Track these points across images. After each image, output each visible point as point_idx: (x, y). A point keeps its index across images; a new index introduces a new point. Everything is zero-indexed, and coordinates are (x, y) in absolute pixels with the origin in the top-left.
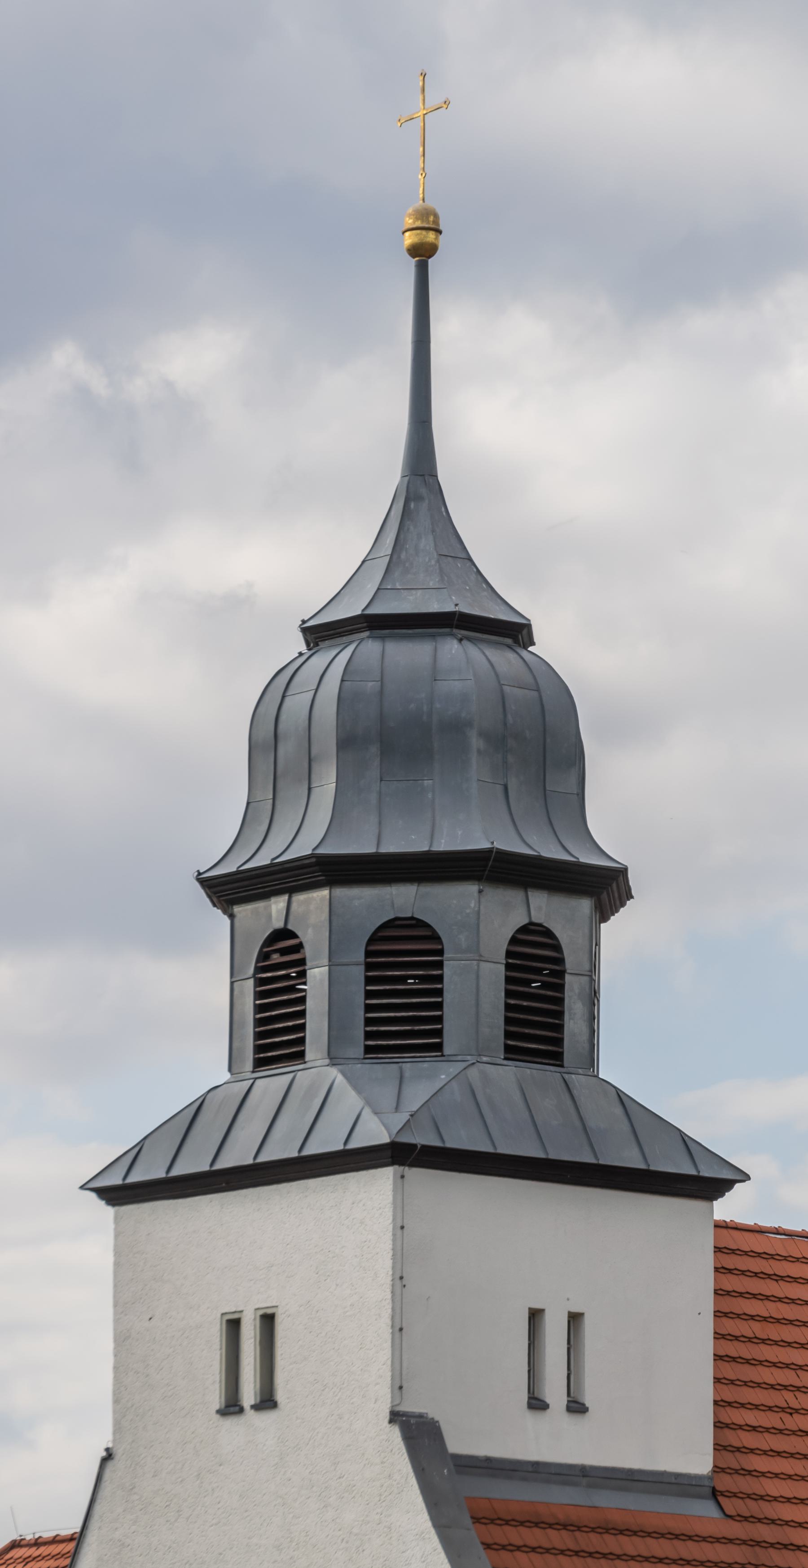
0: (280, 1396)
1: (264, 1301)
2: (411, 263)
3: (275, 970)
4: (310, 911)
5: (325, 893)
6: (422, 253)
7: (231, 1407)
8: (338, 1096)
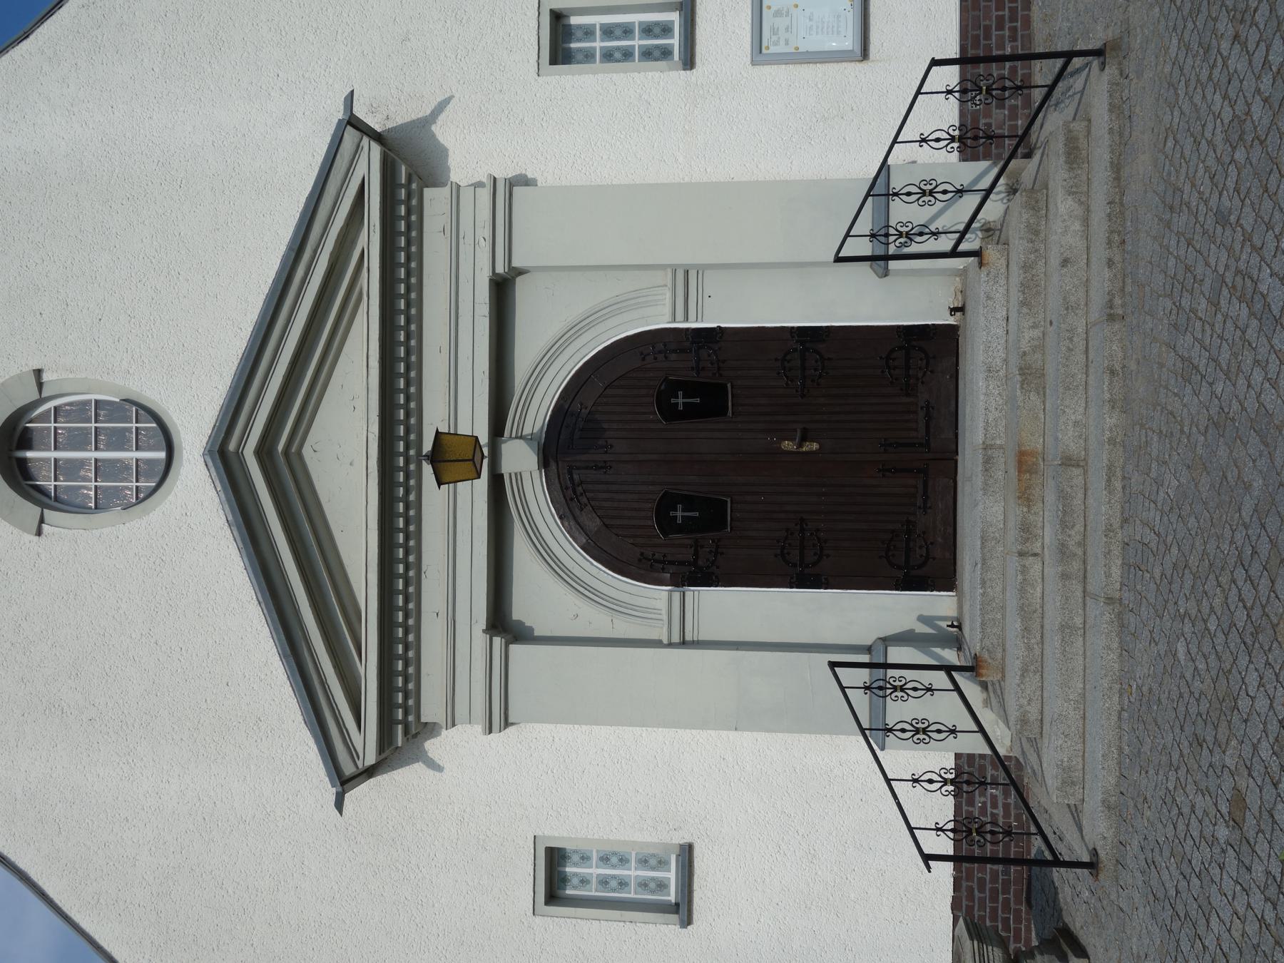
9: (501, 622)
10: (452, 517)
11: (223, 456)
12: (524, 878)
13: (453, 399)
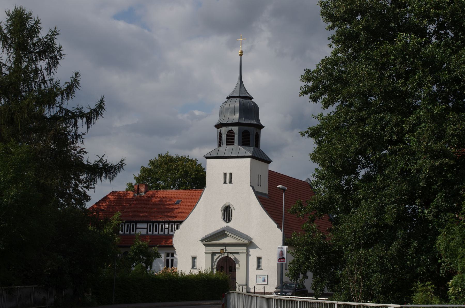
0: (232, 182)
1: (231, 172)
2: (240, 56)
3: (230, 135)
4: (236, 129)
5: (238, 128)
6: (241, 55)
7: (225, 182)
8: (225, 149)
9: (213, 254)
10: (218, 249)
11: (227, 226)
12: (194, 255)
13: (230, 249)
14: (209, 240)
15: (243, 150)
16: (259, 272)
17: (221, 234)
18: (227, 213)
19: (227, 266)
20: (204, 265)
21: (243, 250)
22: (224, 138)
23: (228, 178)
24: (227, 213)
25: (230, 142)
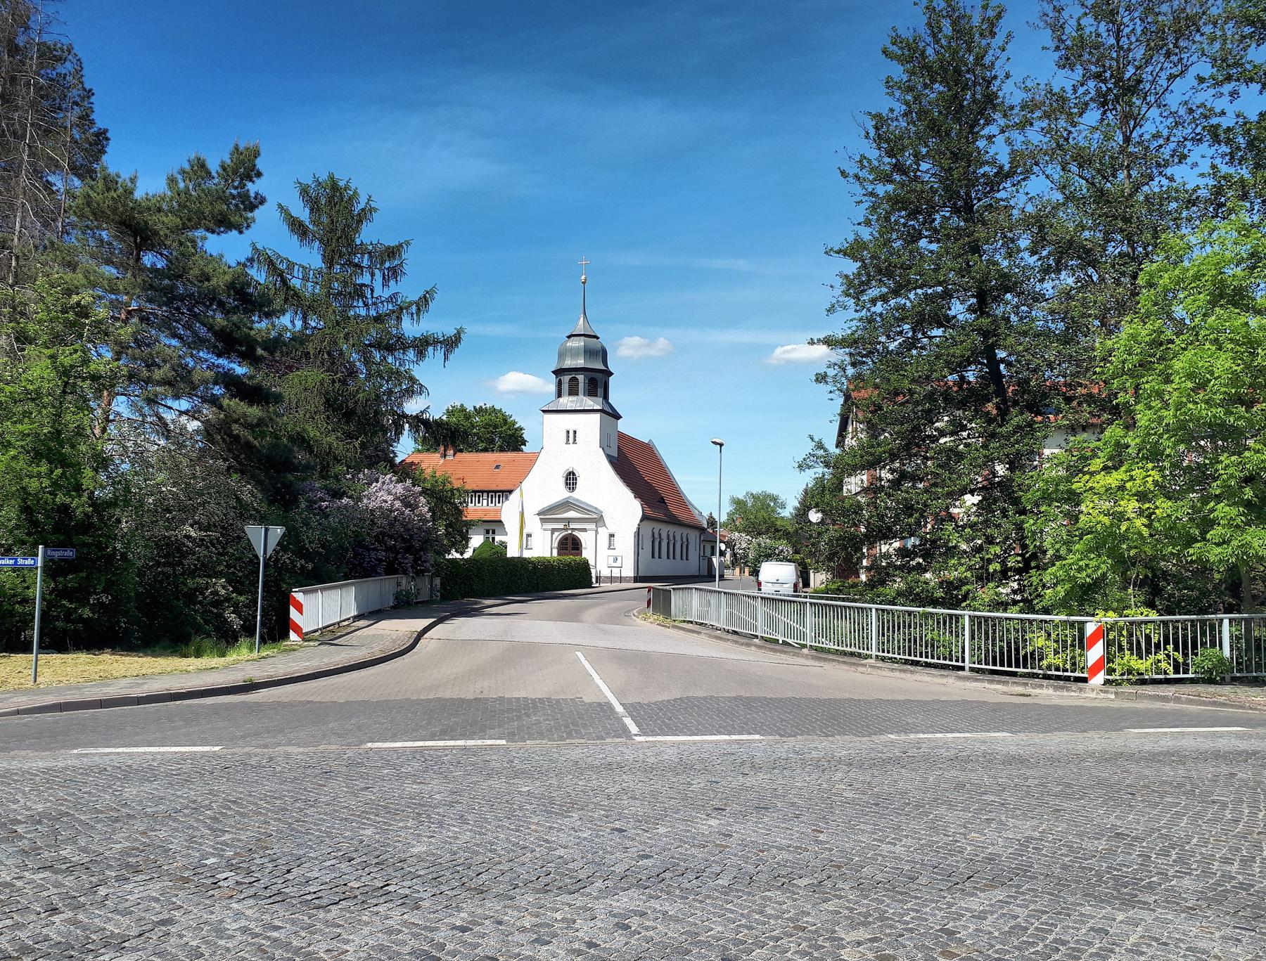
4: (581, 378)
7: (567, 442)
8: (567, 401)
9: (553, 531)
14: (546, 515)
15: (590, 403)
16: (612, 552)
17: (566, 505)
18: (571, 479)
19: (570, 544)
20: (541, 546)
21: (593, 526)
22: (565, 387)
23: (571, 437)
24: (571, 479)
25: (573, 392)
